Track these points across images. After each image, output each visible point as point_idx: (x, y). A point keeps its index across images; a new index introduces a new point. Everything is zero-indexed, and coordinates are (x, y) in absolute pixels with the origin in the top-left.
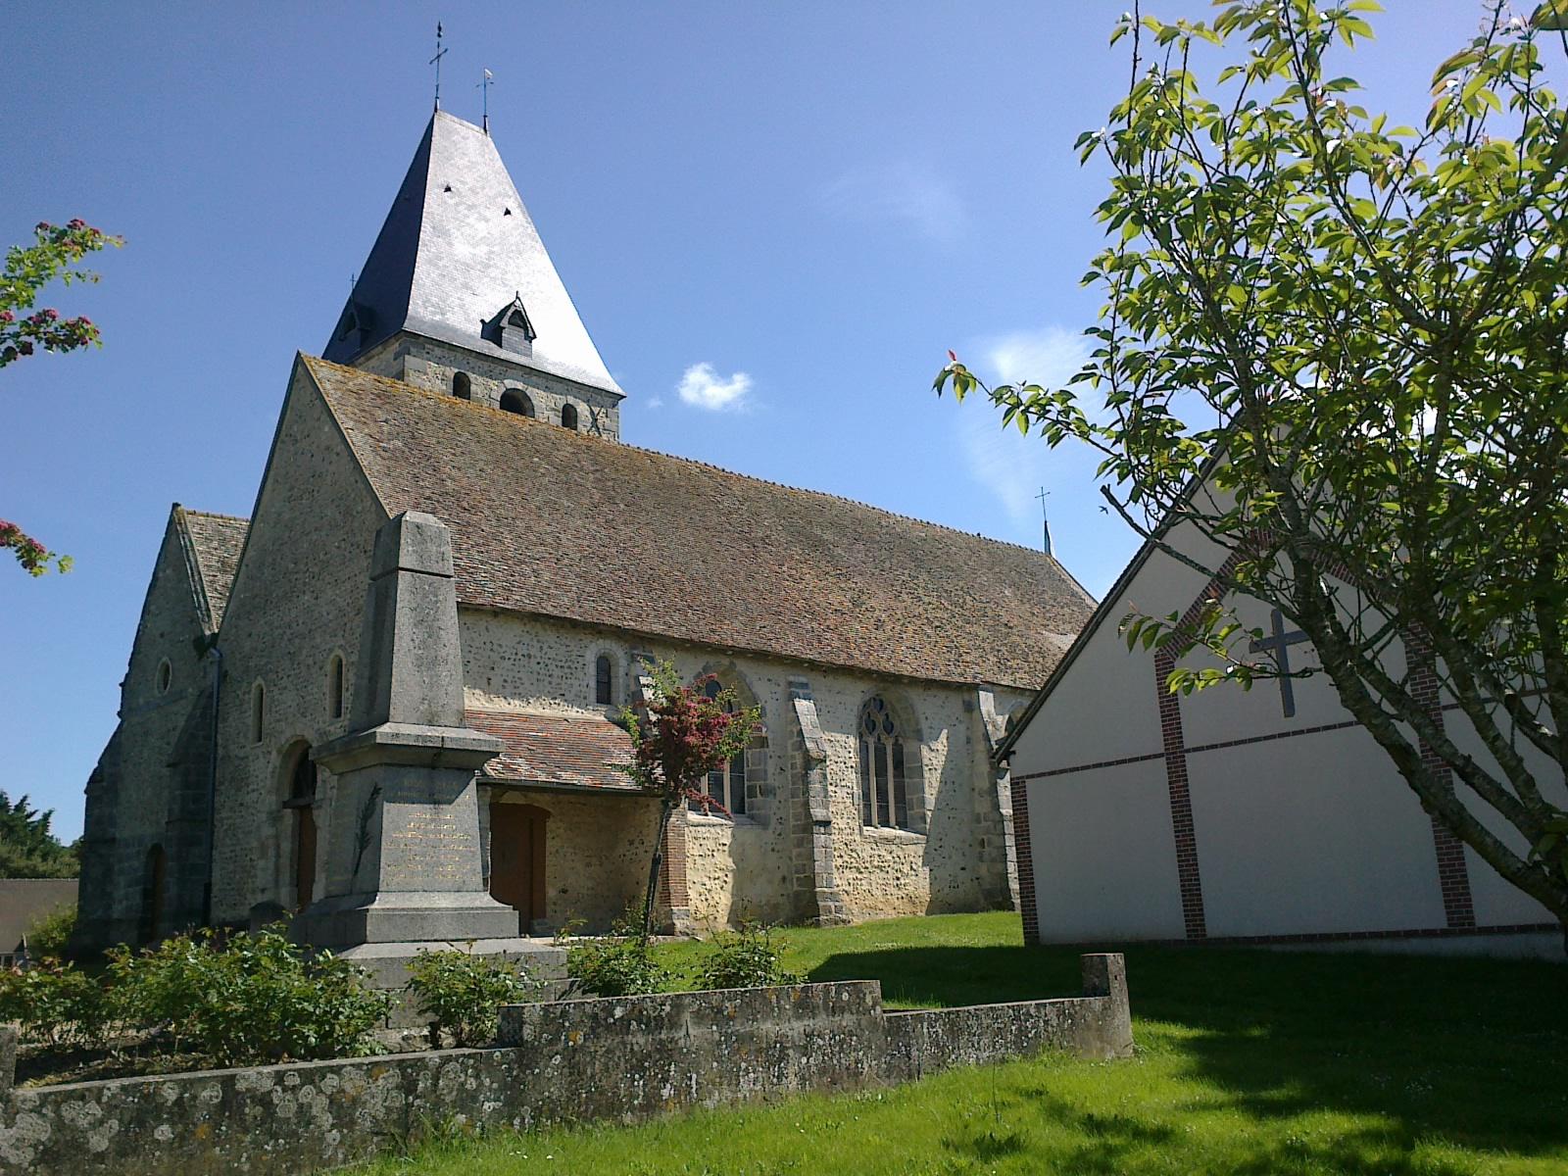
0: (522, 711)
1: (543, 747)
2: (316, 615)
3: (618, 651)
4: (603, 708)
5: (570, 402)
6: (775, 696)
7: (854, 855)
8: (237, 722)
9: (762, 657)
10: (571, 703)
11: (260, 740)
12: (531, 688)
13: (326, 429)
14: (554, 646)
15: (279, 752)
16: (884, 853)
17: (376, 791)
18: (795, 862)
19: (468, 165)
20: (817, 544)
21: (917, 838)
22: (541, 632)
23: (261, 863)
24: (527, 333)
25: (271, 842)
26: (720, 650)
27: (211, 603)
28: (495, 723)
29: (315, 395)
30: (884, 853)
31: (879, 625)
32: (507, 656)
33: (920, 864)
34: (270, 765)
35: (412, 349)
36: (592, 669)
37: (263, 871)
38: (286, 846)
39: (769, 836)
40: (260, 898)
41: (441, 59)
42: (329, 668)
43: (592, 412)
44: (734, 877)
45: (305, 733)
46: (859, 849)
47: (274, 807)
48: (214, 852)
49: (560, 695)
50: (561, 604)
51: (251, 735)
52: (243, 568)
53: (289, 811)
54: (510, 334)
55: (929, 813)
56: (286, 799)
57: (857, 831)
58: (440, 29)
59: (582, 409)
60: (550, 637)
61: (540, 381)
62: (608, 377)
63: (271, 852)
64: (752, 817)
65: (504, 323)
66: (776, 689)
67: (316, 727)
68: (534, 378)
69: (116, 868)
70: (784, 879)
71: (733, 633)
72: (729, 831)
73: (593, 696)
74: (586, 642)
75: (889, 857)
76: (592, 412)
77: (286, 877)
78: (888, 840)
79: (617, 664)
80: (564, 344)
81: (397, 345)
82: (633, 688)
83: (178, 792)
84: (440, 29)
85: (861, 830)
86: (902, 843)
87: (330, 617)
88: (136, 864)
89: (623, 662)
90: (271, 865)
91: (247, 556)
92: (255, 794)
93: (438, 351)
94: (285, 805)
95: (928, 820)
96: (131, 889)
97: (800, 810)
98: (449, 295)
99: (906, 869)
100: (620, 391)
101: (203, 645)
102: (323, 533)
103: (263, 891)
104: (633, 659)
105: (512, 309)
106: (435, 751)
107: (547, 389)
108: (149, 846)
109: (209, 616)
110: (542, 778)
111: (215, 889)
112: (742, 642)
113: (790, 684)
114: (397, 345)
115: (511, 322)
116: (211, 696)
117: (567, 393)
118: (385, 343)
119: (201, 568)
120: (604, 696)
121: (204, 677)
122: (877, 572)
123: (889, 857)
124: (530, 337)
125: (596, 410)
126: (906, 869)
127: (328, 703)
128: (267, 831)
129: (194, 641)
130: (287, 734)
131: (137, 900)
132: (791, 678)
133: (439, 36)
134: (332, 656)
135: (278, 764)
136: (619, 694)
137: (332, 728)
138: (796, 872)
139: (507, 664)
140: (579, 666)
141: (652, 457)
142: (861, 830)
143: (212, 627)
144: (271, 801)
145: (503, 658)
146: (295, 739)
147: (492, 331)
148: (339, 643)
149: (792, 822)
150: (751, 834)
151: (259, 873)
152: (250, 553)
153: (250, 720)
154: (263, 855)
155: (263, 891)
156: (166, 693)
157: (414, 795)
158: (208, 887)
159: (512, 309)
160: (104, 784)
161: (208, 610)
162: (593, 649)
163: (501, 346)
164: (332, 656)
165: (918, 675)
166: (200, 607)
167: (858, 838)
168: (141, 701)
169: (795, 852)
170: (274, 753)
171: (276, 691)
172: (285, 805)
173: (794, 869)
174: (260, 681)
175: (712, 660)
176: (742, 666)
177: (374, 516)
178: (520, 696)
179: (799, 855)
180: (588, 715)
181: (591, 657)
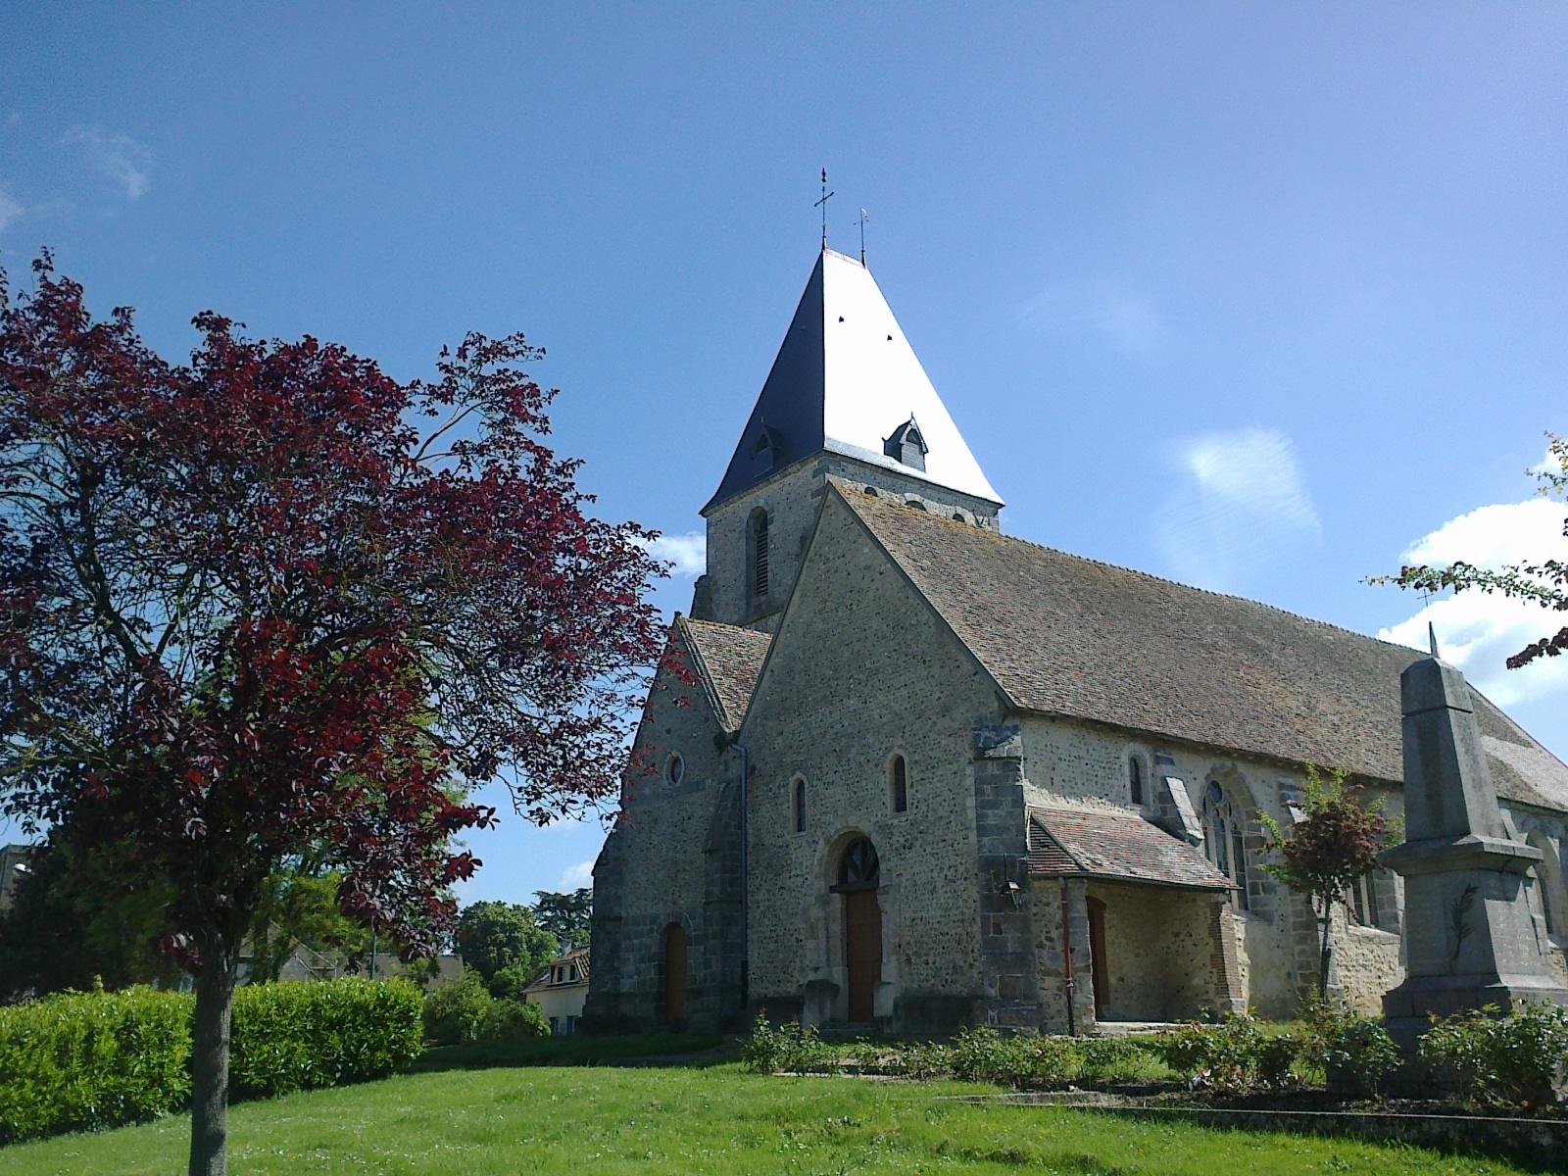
0: (1078, 809)
1: (1109, 845)
2: (865, 717)
3: (1145, 753)
4: (1138, 808)
5: (959, 512)
6: (1269, 798)
7: (1343, 953)
8: (770, 817)
9: (1261, 759)
10: (1113, 802)
11: (800, 830)
12: (1083, 788)
13: (866, 550)
14: (1097, 747)
15: (827, 842)
16: (1366, 952)
17: (1471, 890)
18: (1297, 958)
19: (852, 295)
20: (1256, 650)
21: (1393, 938)
22: (1087, 736)
23: (810, 944)
24: (921, 448)
25: (821, 924)
26: (1226, 752)
27: (724, 703)
28: (1065, 820)
29: (850, 519)
30: (1366, 952)
31: (1336, 728)
32: (1063, 757)
33: (1397, 963)
34: (817, 853)
35: (831, 467)
36: (1126, 769)
37: (813, 951)
38: (837, 928)
39: (1274, 931)
40: (812, 976)
41: (827, 201)
42: (888, 765)
43: (977, 521)
44: (1250, 970)
45: (861, 826)
46: (1346, 947)
47: (823, 892)
48: (749, 931)
49: (1104, 795)
50: (1099, 711)
51: (792, 825)
52: (768, 674)
53: (837, 895)
54: (908, 450)
55: (1401, 913)
56: (834, 882)
57: (1343, 929)
58: (824, 174)
59: (969, 517)
60: (1093, 739)
61: (934, 493)
62: (993, 492)
63: (822, 934)
64: (1256, 914)
65: (903, 440)
66: (1269, 791)
67: (873, 820)
68: (929, 491)
69: (623, 946)
70: (1289, 974)
71: (1230, 736)
72: (1242, 926)
73: (1129, 798)
74: (1119, 744)
75: (1371, 956)
76: (977, 521)
77: (838, 955)
78: (1370, 939)
79: (1145, 766)
80: (951, 462)
81: (816, 463)
82: (1160, 789)
83: (717, 876)
84: (824, 174)
85: (1346, 928)
86: (1382, 943)
87: (884, 720)
88: (648, 941)
89: (1150, 764)
90: (823, 946)
91: (772, 662)
92: (800, 879)
93: (851, 468)
94: (832, 890)
95: (1401, 920)
96: (643, 965)
97: (1300, 907)
98: (854, 417)
99: (1385, 968)
100: (1001, 502)
101: (722, 742)
102: (868, 644)
103: (816, 969)
104: (1158, 760)
105: (909, 428)
106: (1507, 858)
107: (939, 500)
108: (664, 925)
109: (725, 716)
110: (1124, 873)
111: (752, 968)
112: (1242, 743)
113: (1281, 786)
114: (816, 463)
115: (905, 440)
116: (739, 788)
117: (955, 504)
118: (804, 463)
119: (710, 673)
120: (1137, 799)
121: (726, 770)
122: (1312, 675)
123: (1371, 956)
124: (923, 451)
125: (980, 518)
126: (1385, 968)
127: (889, 798)
128: (816, 913)
129: (715, 738)
130: (836, 826)
131: (652, 974)
132: (1281, 780)
133: (824, 180)
134: (891, 754)
135: (826, 853)
136: (1149, 796)
137: (895, 822)
138: (1299, 969)
139: (1064, 765)
140: (1117, 767)
141: (1100, 567)
142: (1346, 928)
143: (731, 725)
144: (820, 886)
145: (1060, 759)
146: (846, 830)
147: (893, 447)
148: (899, 743)
149: (1291, 920)
150: (1260, 928)
151: (808, 953)
152: (775, 660)
153: (789, 810)
154: (813, 935)
155: (816, 969)
156: (678, 784)
157: (1496, 893)
158: (745, 965)
159: (909, 428)
160: (610, 866)
161: (722, 710)
162: (1127, 751)
163: (900, 461)
164: (891, 754)
165: (1386, 777)
166: (715, 708)
167: (1344, 936)
168: (647, 791)
169: (1297, 949)
170: (822, 842)
171: (820, 787)
172: (832, 890)
173: (1296, 966)
174: (799, 775)
175: (1216, 762)
176: (1242, 768)
177: (933, 629)
178: (1076, 795)
179: (1302, 952)
180: (1128, 814)
181: (1125, 759)
